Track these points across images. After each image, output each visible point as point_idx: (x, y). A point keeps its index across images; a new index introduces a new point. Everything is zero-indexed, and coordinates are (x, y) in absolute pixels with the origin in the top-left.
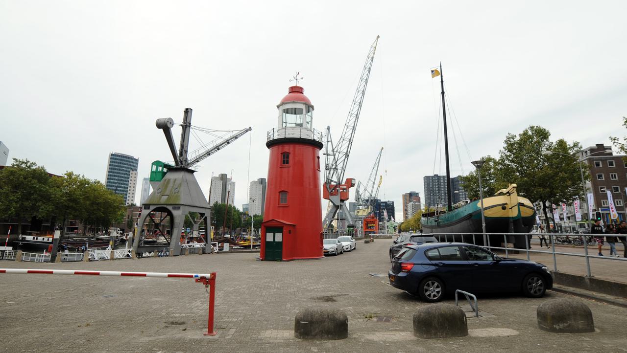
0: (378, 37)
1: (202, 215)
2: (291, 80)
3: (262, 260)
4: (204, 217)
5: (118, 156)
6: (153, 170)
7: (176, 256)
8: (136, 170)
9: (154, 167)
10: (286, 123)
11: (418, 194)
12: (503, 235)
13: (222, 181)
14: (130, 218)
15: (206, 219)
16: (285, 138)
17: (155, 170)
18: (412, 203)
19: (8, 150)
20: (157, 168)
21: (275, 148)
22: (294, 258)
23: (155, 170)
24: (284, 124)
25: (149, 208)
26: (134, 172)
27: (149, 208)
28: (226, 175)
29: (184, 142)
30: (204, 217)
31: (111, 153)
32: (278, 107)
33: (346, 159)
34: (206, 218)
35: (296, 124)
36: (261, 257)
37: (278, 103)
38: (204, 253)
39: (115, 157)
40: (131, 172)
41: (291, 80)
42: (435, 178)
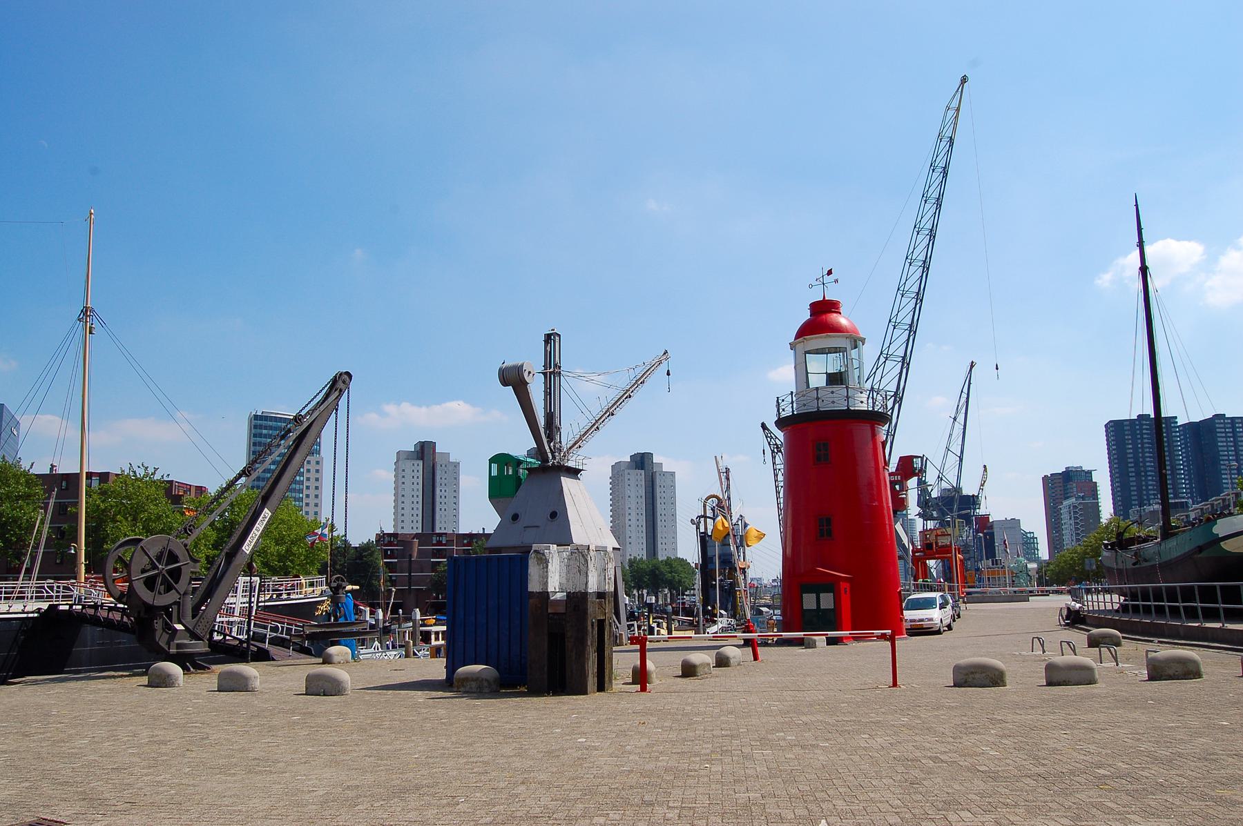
0: (964, 80)
2: (811, 286)
5: (271, 419)
9: (495, 466)
11: (1089, 473)
12: (1215, 587)
13: (421, 463)
18: (1074, 500)
26: (316, 457)
33: (897, 406)
35: (826, 373)
41: (811, 286)
42: (1141, 425)
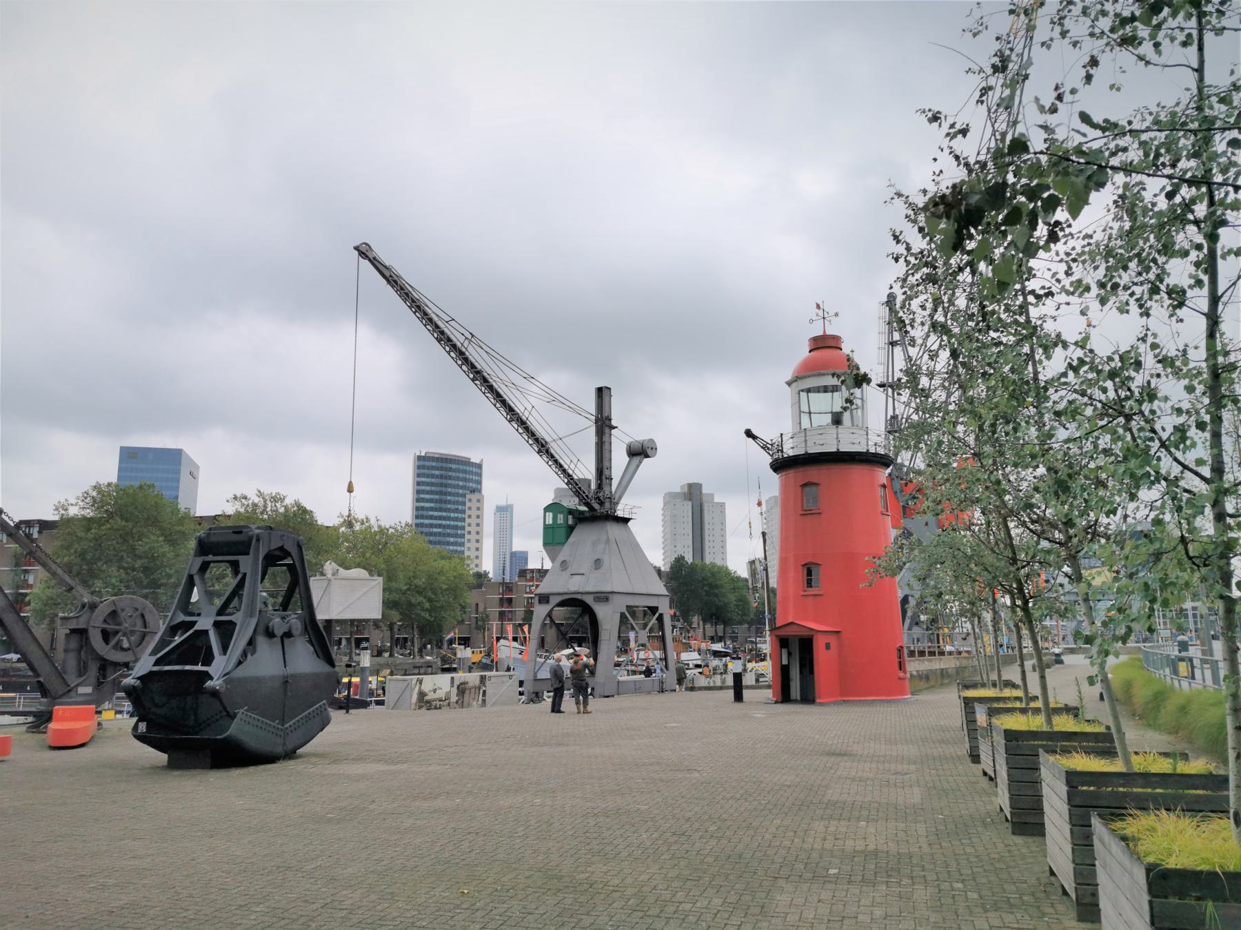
1: (653, 610)
2: (812, 321)
3: (776, 702)
4: (657, 615)
6: (547, 523)
7: (608, 697)
8: (480, 491)
9: (550, 516)
10: (810, 413)
14: (481, 609)
15: (660, 619)
16: (806, 454)
17: (551, 522)
19: (197, 467)
20: (555, 518)
21: (791, 473)
22: (850, 698)
23: (551, 522)
24: (805, 418)
25: (548, 602)
27: (548, 602)
28: (699, 486)
29: (602, 461)
30: (657, 615)
31: (418, 454)
32: (789, 384)
34: (661, 616)
36: (773, 697)
37: (789, 377)
38: (662, 691)
39: (427, 464)
40: (468, 497)
